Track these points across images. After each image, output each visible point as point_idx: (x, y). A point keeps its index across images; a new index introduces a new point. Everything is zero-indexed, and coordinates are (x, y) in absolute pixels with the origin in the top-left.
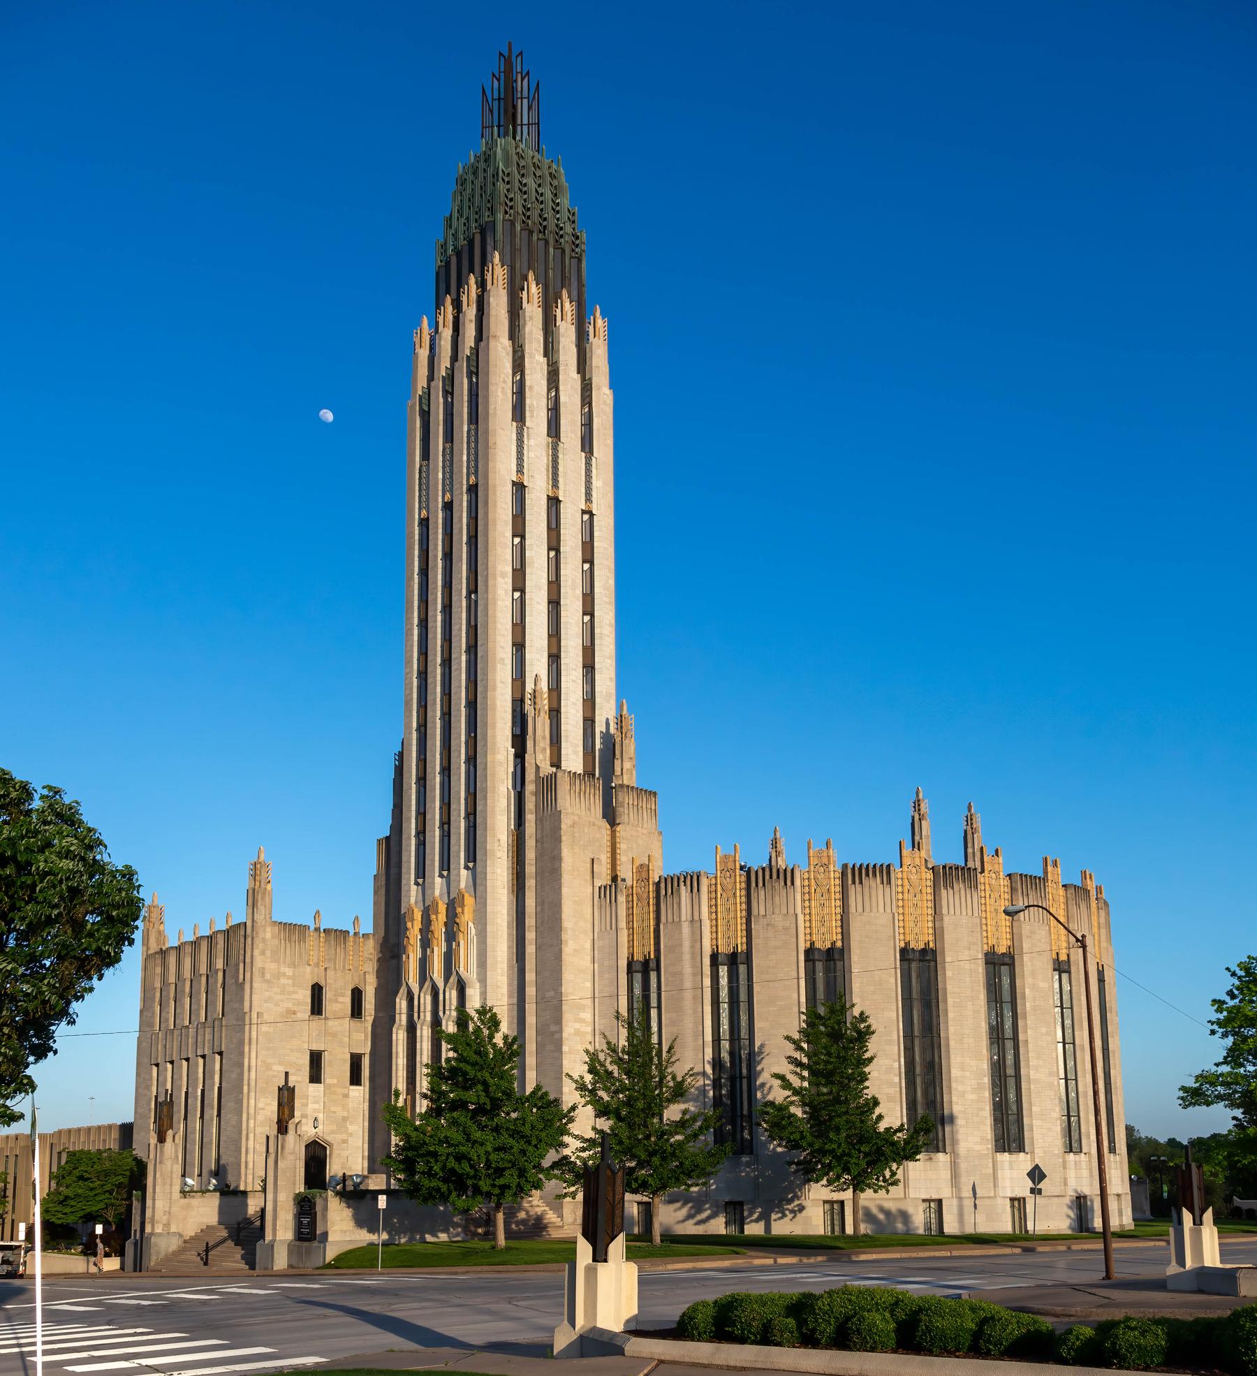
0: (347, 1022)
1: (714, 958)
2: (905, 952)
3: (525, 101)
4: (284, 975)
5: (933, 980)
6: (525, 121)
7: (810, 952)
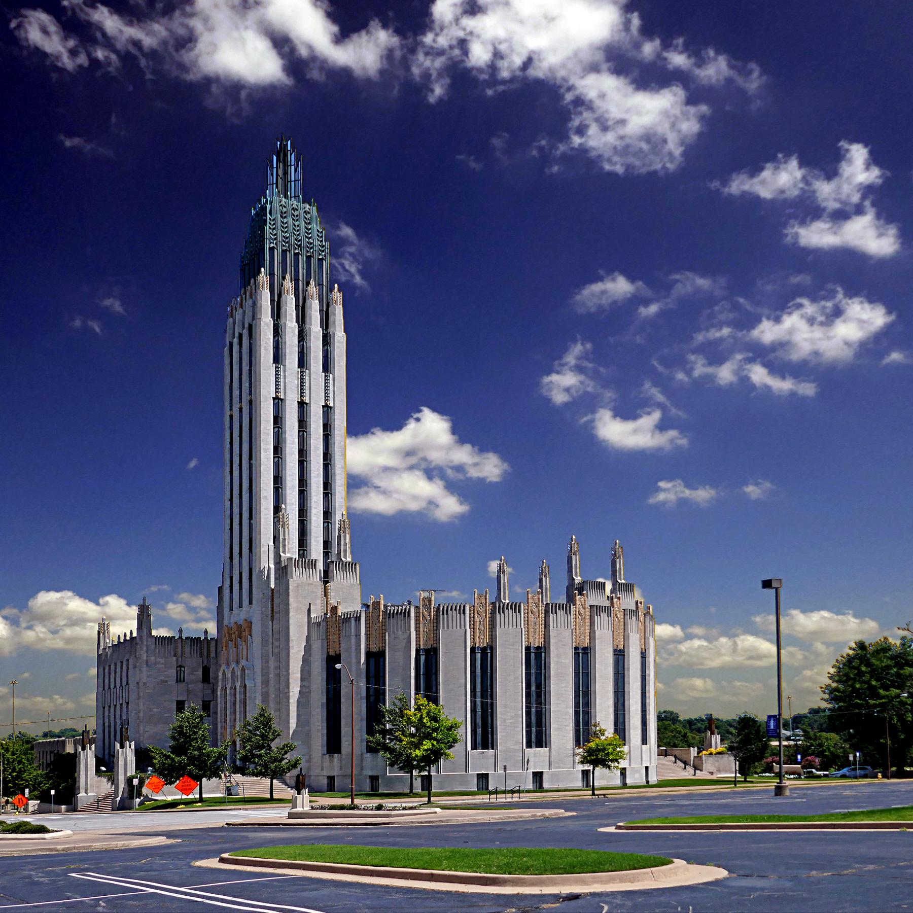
0: (200, 685)
1: (473, 650)
2: (576, 649)
3: (293, 167)
4: (159, 663)
5: (381, 670)
6: (293, 179)
7: (528, 648)
